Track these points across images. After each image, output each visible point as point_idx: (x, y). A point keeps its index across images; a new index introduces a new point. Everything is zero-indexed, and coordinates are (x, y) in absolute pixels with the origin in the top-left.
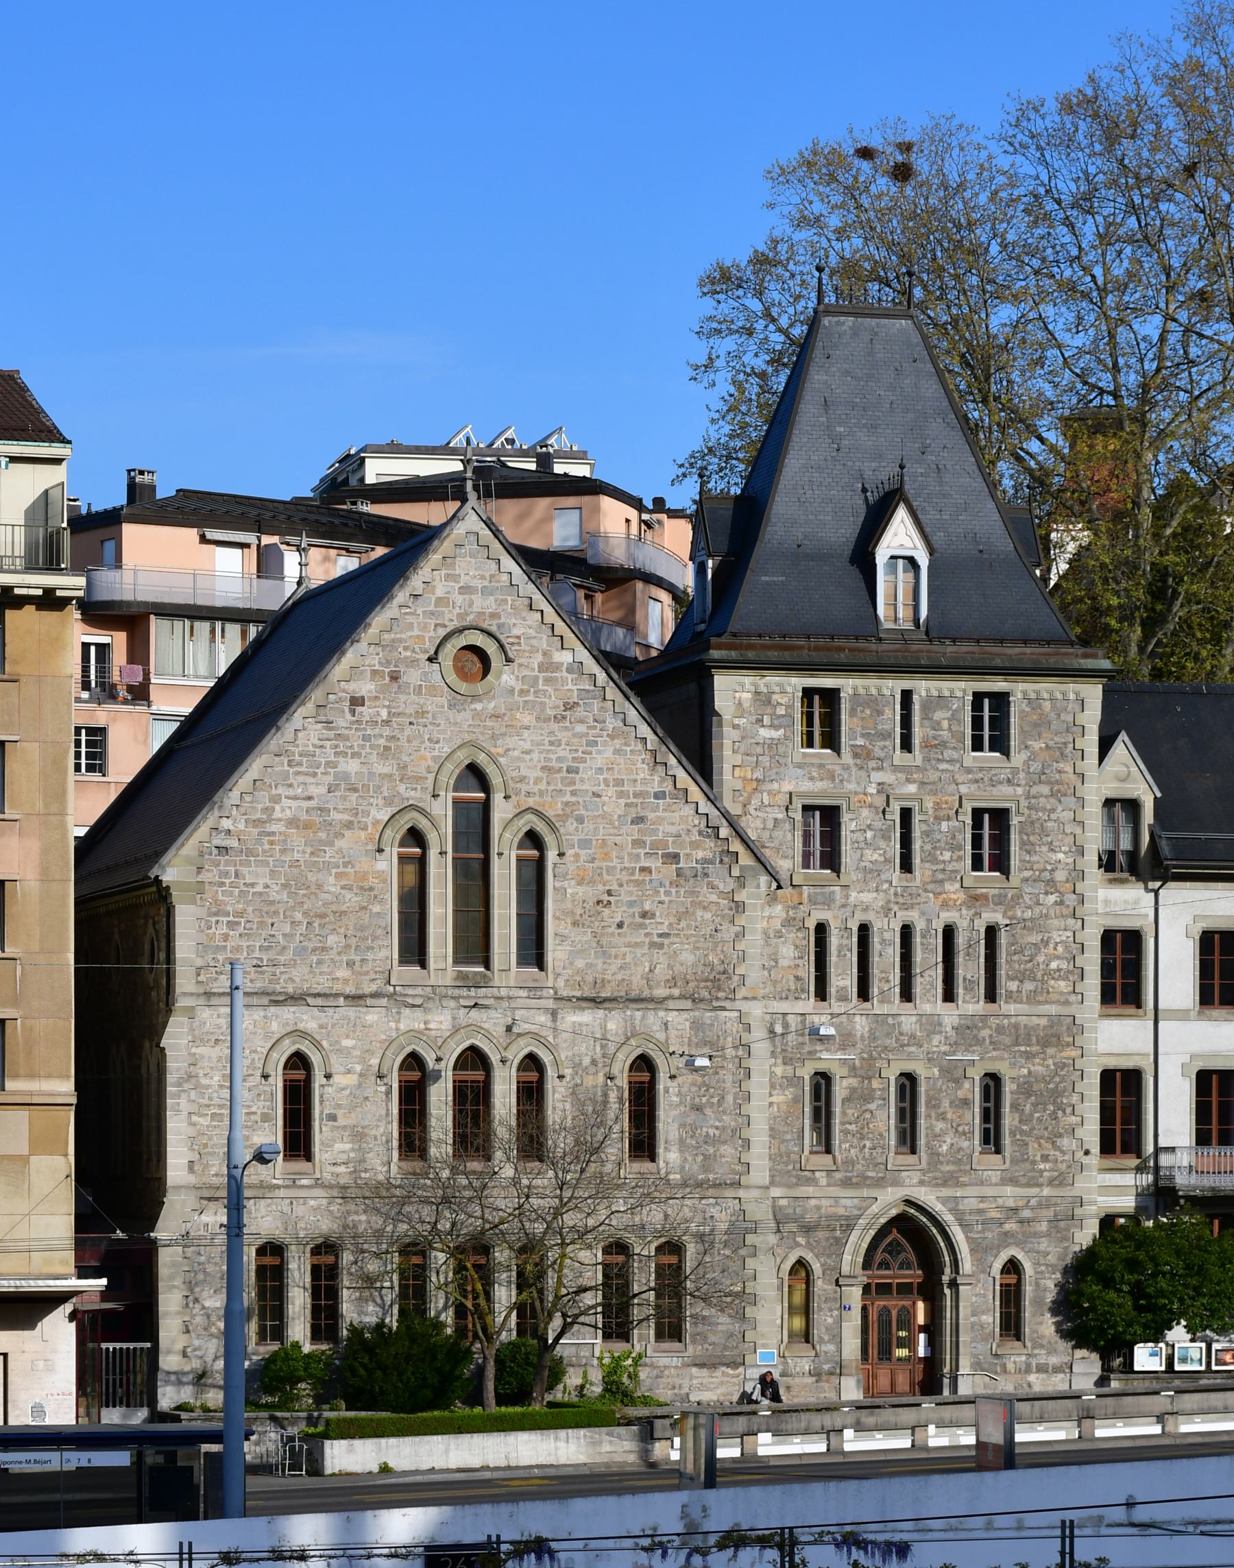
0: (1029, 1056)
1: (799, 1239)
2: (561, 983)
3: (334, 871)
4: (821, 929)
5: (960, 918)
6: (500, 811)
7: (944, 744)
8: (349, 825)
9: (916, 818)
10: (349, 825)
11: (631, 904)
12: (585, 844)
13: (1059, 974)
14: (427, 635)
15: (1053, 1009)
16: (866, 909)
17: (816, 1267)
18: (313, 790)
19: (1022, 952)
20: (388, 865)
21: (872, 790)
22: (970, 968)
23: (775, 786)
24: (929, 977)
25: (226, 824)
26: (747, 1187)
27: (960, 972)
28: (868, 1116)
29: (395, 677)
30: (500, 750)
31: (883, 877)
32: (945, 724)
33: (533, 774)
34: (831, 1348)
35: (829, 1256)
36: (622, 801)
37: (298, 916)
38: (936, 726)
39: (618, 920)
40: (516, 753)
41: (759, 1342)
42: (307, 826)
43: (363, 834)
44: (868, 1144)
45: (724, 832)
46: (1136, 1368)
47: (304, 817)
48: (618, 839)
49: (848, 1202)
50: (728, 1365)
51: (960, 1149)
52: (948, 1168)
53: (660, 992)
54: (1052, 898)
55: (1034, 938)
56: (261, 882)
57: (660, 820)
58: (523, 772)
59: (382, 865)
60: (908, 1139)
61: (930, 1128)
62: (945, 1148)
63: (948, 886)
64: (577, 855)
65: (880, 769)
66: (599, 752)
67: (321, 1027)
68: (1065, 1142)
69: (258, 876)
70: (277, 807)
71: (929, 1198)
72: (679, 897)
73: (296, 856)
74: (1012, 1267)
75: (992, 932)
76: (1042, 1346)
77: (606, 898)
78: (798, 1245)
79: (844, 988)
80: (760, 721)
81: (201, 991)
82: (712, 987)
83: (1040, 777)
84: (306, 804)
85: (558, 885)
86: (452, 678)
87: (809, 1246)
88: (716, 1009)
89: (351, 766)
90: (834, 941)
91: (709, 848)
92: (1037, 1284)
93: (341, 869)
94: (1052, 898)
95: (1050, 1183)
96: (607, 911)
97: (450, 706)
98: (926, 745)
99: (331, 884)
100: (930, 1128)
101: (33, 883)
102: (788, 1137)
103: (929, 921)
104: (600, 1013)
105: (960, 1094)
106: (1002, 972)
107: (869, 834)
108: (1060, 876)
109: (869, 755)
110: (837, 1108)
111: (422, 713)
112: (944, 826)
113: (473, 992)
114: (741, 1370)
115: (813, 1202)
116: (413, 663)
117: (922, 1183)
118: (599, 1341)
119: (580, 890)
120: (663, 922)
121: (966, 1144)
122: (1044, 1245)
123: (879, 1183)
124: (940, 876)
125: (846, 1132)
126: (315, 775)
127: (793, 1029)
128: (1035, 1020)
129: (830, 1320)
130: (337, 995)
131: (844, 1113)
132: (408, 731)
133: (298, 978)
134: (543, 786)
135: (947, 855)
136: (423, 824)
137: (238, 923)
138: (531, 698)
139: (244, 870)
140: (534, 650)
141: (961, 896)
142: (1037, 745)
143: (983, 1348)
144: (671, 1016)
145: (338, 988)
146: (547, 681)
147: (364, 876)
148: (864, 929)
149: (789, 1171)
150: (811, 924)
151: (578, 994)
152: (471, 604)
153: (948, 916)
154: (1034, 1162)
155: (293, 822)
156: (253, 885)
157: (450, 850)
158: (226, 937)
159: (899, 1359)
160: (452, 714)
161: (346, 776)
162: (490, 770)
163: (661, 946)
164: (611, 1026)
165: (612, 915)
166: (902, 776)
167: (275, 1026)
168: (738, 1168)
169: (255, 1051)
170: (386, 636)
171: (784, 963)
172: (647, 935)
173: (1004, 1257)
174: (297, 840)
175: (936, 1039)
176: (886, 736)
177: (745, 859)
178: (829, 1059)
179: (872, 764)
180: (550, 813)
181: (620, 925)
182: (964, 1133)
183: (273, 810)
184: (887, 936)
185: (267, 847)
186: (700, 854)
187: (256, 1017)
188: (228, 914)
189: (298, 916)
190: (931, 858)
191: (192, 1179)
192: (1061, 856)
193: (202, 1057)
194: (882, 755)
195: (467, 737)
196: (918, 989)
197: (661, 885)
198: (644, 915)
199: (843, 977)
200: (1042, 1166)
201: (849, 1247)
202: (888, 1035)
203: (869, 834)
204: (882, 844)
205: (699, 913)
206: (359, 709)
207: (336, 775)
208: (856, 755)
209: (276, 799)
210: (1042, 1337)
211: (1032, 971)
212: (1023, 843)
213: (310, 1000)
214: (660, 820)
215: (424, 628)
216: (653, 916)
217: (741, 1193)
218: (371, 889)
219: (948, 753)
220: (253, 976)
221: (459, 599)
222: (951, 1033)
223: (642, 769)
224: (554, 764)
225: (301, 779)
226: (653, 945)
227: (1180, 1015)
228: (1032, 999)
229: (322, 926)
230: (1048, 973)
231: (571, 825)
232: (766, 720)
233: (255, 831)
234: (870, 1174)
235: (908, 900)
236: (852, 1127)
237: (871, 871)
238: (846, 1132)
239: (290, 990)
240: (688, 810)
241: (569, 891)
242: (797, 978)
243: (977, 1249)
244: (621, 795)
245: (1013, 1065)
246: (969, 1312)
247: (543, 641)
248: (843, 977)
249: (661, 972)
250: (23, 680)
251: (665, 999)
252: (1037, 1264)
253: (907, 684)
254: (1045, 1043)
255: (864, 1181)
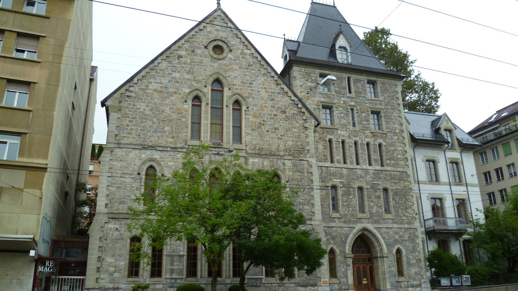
0: (396, 183)
1: (331, 241)
2: (248, 148)
3: (169, 107)
4: (330, 141)
5: (371, 141)
6: (227, 93)
7: (360, 92)
8: (175, 93)
9: (355, 112)
10: (175, 93)
11: (271, 125)
12: (256, 105)
13: (400, 159)
14: (204, 41)
15: (401, 169)
16: (343, 136)
17: (337, 251)
18: (163, 81)
19: (389, 152)
20: (188, 106)
21: (342, 102)
22: (375, 156)
23: (313, 99)
24: (363, 156)
25: (131, 89)
26: (315, 221)
27: (372, 157)
28: (350, 200)
29: (193, 51)
30: (227, 75)
31: (347, 127)
32: (360, 87)
33: (238, 83)
34: (345, 280)
35: (341, 247)
36: (267, 94)
37: (155, 120)
38: (358, 87)
39: (267, 129)
40: (233, 77)
41: (322, 277)
42: (161, 92)
43: (180, 96)
44: (351, 209)
45: (300, 106)
46: (442, 285)
47: (159, 89)
48: (266, 105)
49: (346, 229)
50: (311, 286)
51: (379, 212)
52: (376, 218)
53: (282, 153)
54: (396, 137)
55: (393, 148)
56: (142, 108)
57: (280, 101)
58: (235, 83)
59: (186, 106)
60: (362, 210)
61: (369, 205)
62: (374, 211)
63: (366, 132)
64: (253, 109)
65: (343, 97)
66: (259, 79)
67: (161, 158)
68: (409, 210)
69: (142, 106)
70: (150, 85)
71: (370, 227)
72: (286, 124)
73: (156, 101)
74: (399, 251)
75: (380, 145)
76: (411, 278)
77: (263, 122)
78: (331, 243)
79: (339, 159)
80: (307, 80)
81: (117, 142)
82: (298, 152)
83: (388, 104)
84: (160, 85)
85: (247, 117)
86: (212, 53)
87: (334, 244)
88: (300, 160)
89: (177, 75)
90: (334, 145)
91: (295, 110)
92: (407, 257)
93: (171, 106)
94: (396, 137)
95: (407, 223)
96: (263, 127)
97: (211, 61)
98: (356, 92)
99: (167, 110)
100: (369, 205)
101: (43, 85)
102: (325, 206)
103: (362, 141)
104: (261, 159)
105: (377, 194)
106: (384, 158)
107: (342, 115)
108: (397, 131)
109: (340, 93)
110: (340, 197)
111: (201, 62)
112: (363, 115)
113: (217, 150)
114: (316, 287)
115: (335, 228)
116: (200, 48)
117: (368, 223)
118: (264, 277)
119: (254, 120)
120: (281, 132)
121: (380, 210)
122: (408, 244)
123: (355, 222)
124: (364, 128)
125: (343, 205)
126: (164, 77)
127: (324, 171)
128: (396, 173)
129: (343, 270)
130: (168, 147)
131: (342, 199)
132: (197, 67)
133: (153, 140)
134: (241, 87)
135: (365, 123)
136: (200, 94)
137: (133, 121)
138: (237, 62)
139: (137, 104)
140: (238, 48)
141: (370, 135)
142: (386, 95)
143: (393, 279)
144: (286, 162)
145: (169, 145)
146: (242, 57)
147: (179, 109)
148: (343, 142)
149: (326, 217)
150: (327, 139)
151: (254, 152)
152: (219, 34)
153: (367, 140)
154: (401, 217)
155: (155, 90)
156: (139, 109)
157: (210, 103)
158: (128, 125)
159: (364, 284)
160: (211, 63)
161: (175, 78)
162: (224, 81)
163: (282, 139)
164: (265, 163)
165: (264, 128)
166: (350, 100)
167: (143, 156)
168: (311, 214)
169: (135, 165)
170: (191, 40)
171: (320, 150)
172: (277, 135)
173: (396, 247)
174: (156, 95)
175: (368, 177)
176: (345, 88)
177: (307, 114)
178: (336, 181)
179: (341, 95)
180: (244, 96)
181: (268, 131)
182: (379, 207)
183: (149, 86)
184: (350, 144)
185: (145, 97)
186: (293, 112)
187: (136, 152)
188: (129, 118)
189: (155, 120)
190: (360, 123)
191: (106, 211)
192: (397, 126)
193: (115, 165)
194: (344, 93)
195: (216, 71)
196: (361, 161)
197: (281, 120)
198: (275, 129)
199: (338, 156)
200: (404, 218)
201: (347, 244)
202: (354, 175)
203: (342, 115)
204: (346, 117)
205: (294, 129)
206: (180, 59)
207: (171, 78)
208: (336, 93)
209: (150, 83)
210: (411, 275)
211: (393, 158)
212: (386, 121)
213: (157, 148)
214: (280, 101)
215: (204, 39)
216: (278, 129)
217: (313, 223)
218: (182, 113)
219: (362, 95)
220: (137, 139)
221: (215, 32)
222: (372, 175)
223: (274, 86)
224: (245, 81)
225: (159, 77)
226: (279, 139)
227: (424, 183)
228: (394, 165)
229: (163, 124)
230: (397, 158)
231: (250, 100)
232: (309, 81)
233: (142, 92)
234: (352, 219)
235: (355, 133)
236: (345, 204)
237: (344, 125)
238: (343, 205)
239: (150, 144)
240: (287, 98)
241: (250, 119)
242: (324, 155)
243: (388, 245)
244: (267, 92)
245: (391, 186)
246: (388, 266)
247: (241, 46)
248: (338, 156)
249: (282, 147)
250: (51, 18)
251: (284, 156)
252: (406, 250)
253: (349, 75)
254: (400, 180)
255: (350, 222)
